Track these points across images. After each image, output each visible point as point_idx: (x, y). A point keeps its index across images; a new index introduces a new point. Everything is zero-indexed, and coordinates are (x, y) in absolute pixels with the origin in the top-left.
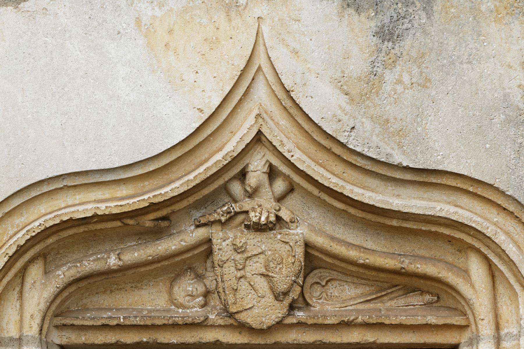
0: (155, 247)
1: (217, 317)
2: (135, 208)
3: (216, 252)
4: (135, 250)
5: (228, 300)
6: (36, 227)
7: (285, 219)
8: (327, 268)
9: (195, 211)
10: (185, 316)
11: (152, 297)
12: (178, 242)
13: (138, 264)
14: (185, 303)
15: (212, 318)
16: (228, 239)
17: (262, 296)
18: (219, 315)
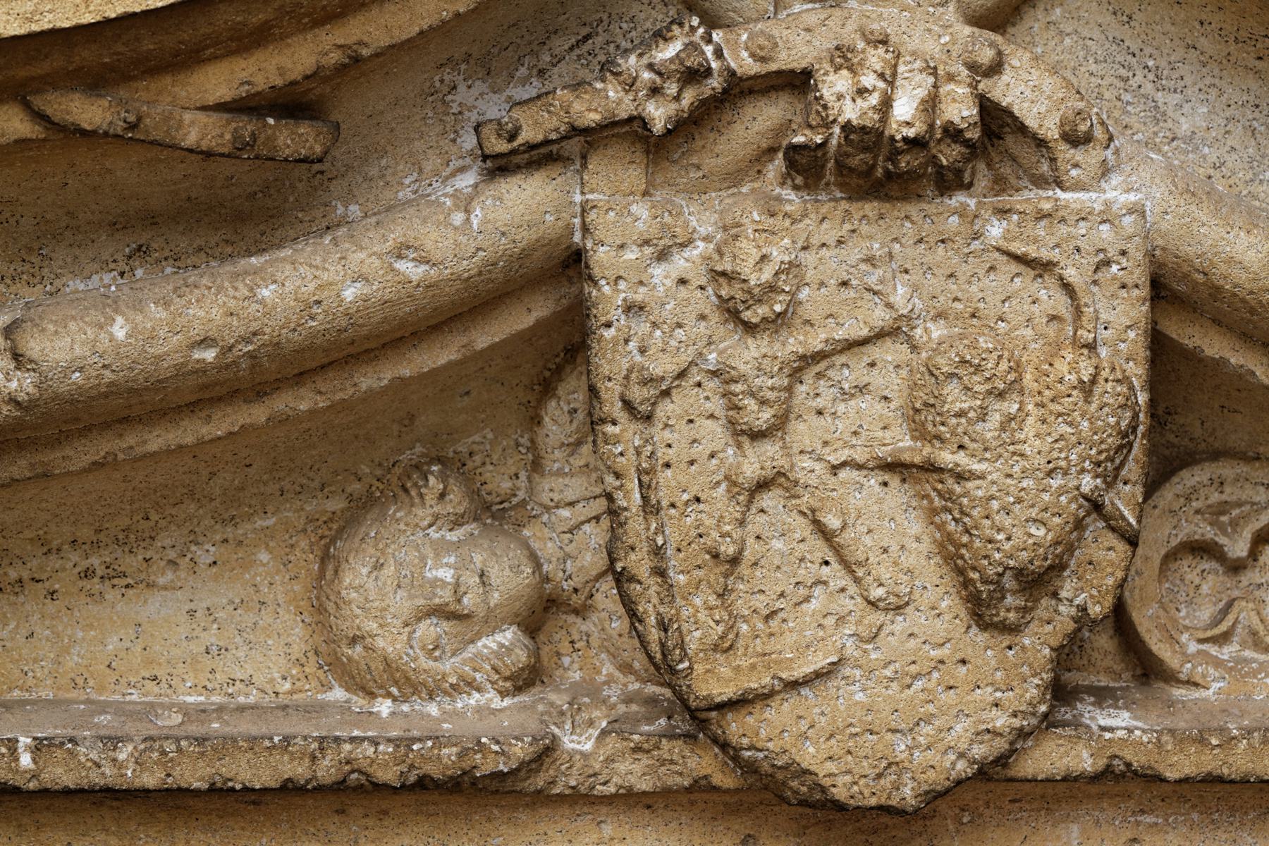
0: (241, 286)
1: (613, 742)
2: (120, 10)
3: (608, 325)
5: (685, 627)
7: (1031, 123)
8: (1258, 459)
9: (479, 86)
10: (415, 733)
11: (211, 637)
12: (379, 256)
13: (131, 391)
14: (415, 659)
15: (581, 753)
16: (683, 245)
17: (892, 599)
18: (619, 733)
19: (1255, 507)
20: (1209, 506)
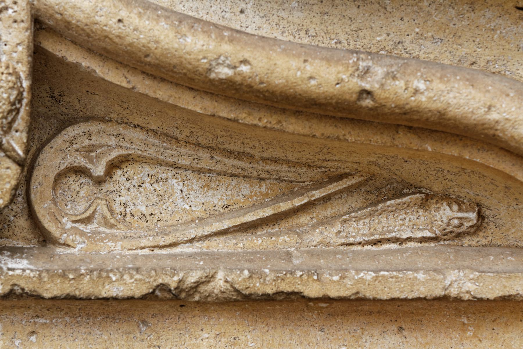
8: (111, 121)
19: (109, 148)
20: (83, 147)
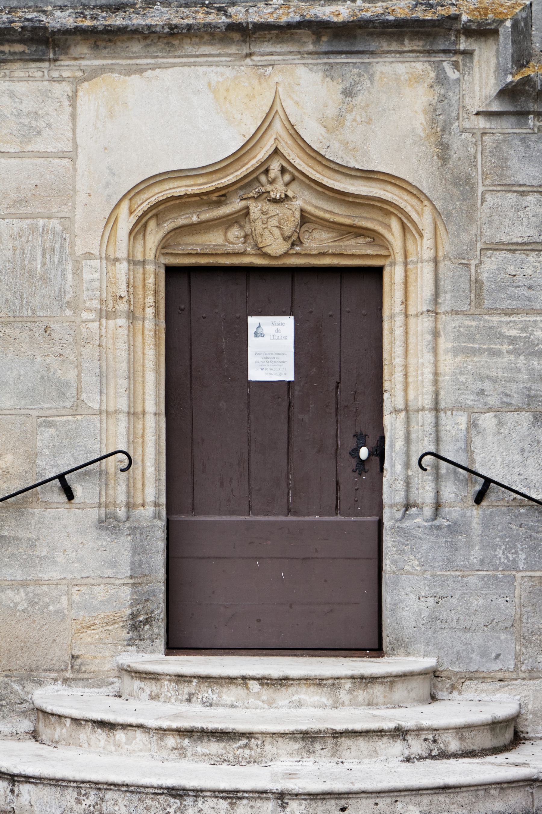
4: (207, 213)
6: (153, 200)
